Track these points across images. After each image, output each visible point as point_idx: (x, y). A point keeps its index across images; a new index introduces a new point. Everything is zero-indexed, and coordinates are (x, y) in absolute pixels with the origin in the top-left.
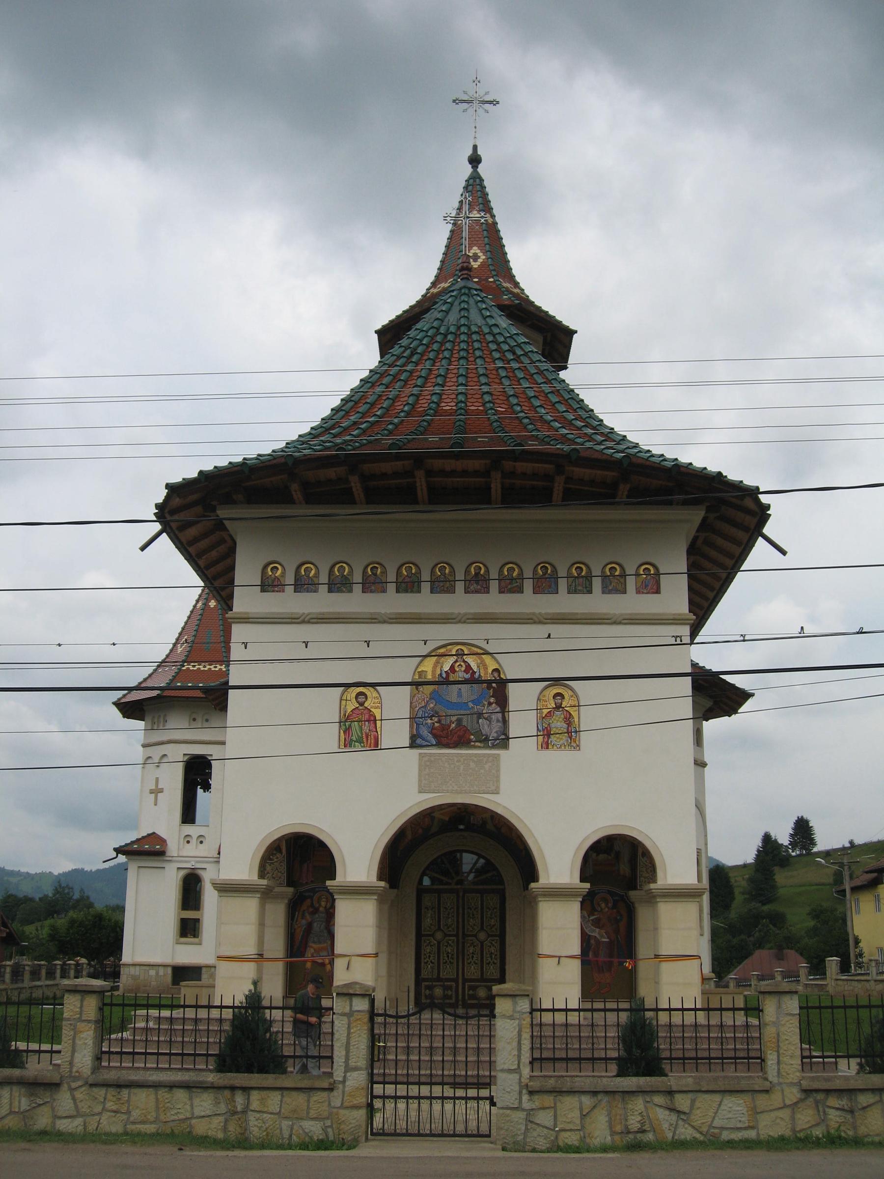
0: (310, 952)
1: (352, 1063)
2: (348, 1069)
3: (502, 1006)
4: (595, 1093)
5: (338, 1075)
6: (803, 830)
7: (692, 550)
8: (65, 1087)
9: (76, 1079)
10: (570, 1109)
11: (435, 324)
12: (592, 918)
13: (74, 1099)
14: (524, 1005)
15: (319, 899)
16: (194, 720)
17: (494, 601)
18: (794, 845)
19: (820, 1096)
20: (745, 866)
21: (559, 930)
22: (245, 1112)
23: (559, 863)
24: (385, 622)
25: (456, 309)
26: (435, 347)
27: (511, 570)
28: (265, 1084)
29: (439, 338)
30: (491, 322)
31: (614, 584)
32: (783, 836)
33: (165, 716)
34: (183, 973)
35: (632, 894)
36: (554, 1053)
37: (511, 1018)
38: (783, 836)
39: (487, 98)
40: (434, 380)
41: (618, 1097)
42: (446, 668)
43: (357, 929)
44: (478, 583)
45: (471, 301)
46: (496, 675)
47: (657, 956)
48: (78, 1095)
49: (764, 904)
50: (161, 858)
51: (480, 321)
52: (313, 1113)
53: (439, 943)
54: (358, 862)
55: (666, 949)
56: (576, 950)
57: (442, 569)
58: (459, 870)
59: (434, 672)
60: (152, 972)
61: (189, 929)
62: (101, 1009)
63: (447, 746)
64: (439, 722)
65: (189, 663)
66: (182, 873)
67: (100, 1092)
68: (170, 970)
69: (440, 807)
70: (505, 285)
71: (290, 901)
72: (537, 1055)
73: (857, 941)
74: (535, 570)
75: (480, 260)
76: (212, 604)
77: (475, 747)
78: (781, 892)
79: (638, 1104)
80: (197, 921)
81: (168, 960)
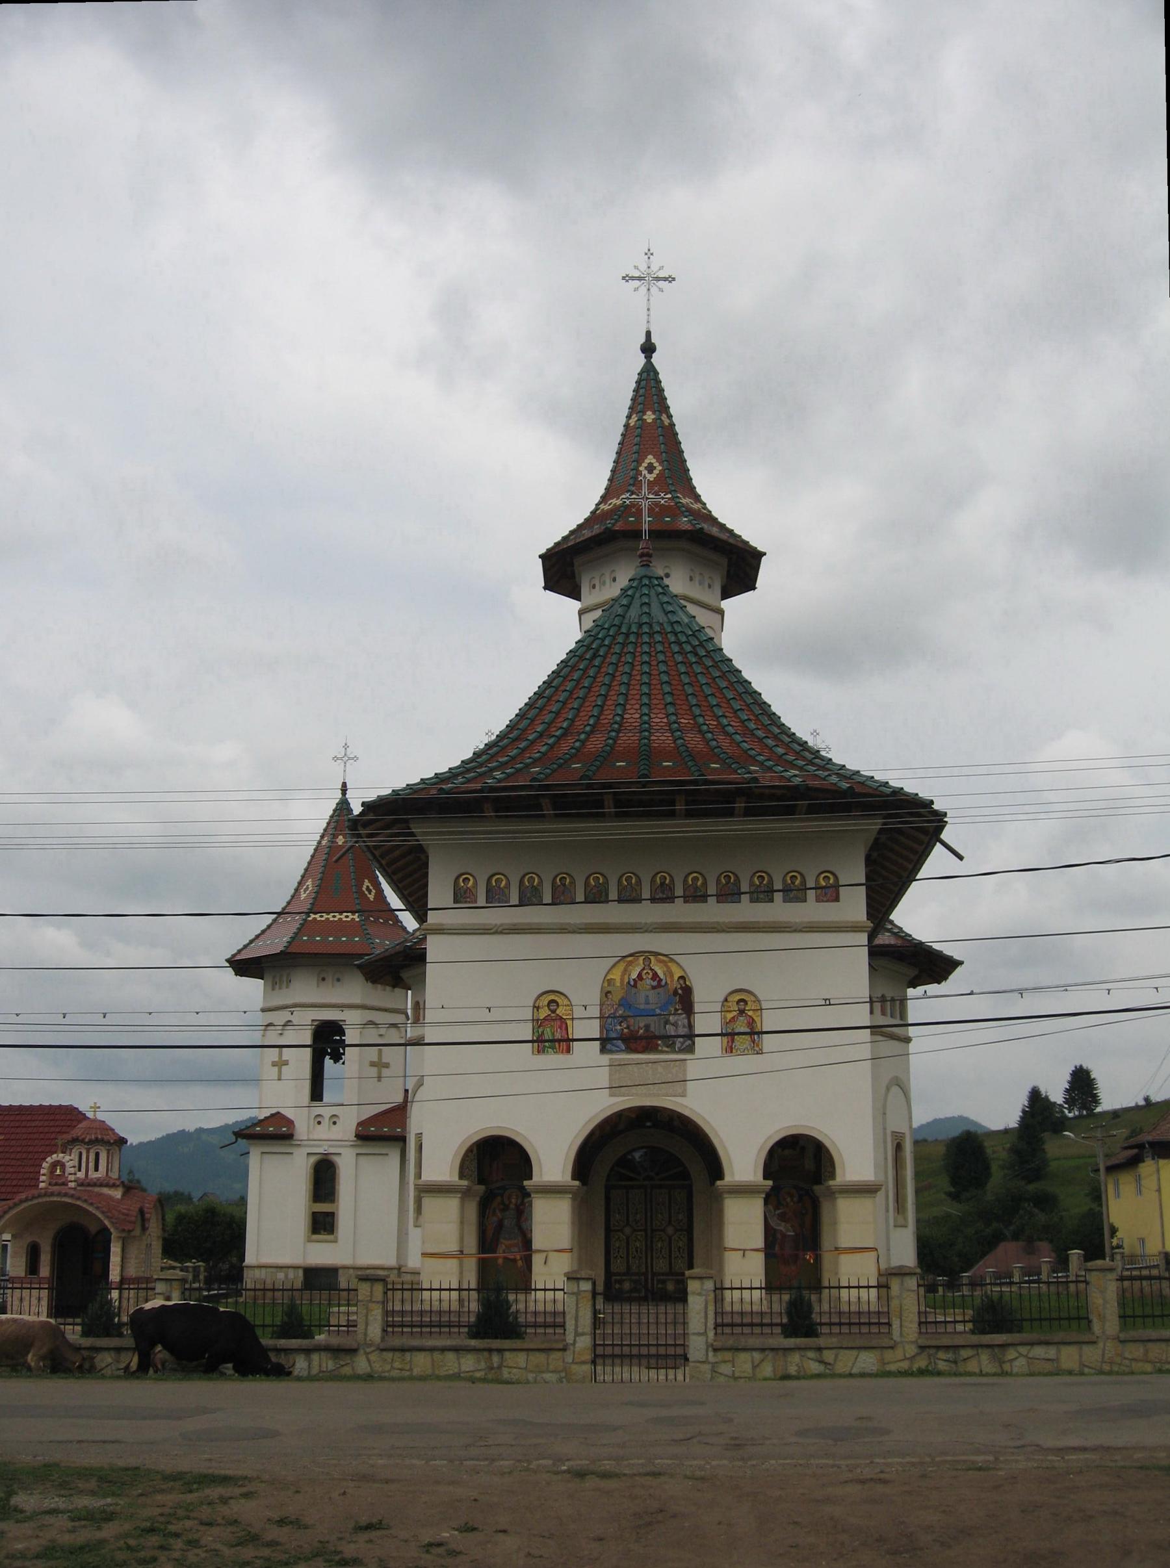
0: (501, 1248)
1: (580, 1330)
2: (577, 1334)
3: (693, 1286)
4: (763, 1350)
5: (570, 1338)
6: (1082, 1084)
7: (869, 861)
8: (362, 1351)
9: (370, 1345)
10: (744, 1362)
11: (617, 622)
12: (778, 1212)
13: (369, 1360)
14: (709, 1285)
15: (509, 1198)
16: (324, 979)
17: (678, 912)
18: (1070, 1101)
19: (932, 1351)
20: (1006, 1131)
21: (744, 1225)
22: (500, 1367)
23: (743, 1162)
24: (574, 932)
25: (637, 603)
26: (617, 649)
27: (695, 879)
28: (514, 1346)
29: (620, 639)
30: (674, 618)
31: (795, 893)
32: (1056, 1094)
33: (288, 975)
34: (319, 1279)
35: (816, 1188)
36: (731, 1327)
37: (699, 1294)
38: (1056, 1094)
39: (661, 274)
40: (617, 688)
41: (780, 1353)
42: (634, 975)
43: (553, 1225)
44: (663, 894)
45: (653, 593)
46: (682, 982)
47: (837, 1249)
48: (373, 1357)
49: (1030, 1182)
50: (287, 1142)
51: (662, 618)
52: (551, 1367)
53: (628, 1238)
54: (553, 1163)
55: (844, 1242)
56: (760, 1244)
57: (629, 879)
58: (648, 1170)
59: (622, 980)
60: (281, 1275)
61: (322, 1224)
62: (385, 1293)
63: (636, 1051)
64: (628, 1027)
65: (315, 913)
66: (313, 1159)
67: (389, 1355)
68: (301, 1273)
69: (630, 1109)
70: (684, 501)
71: (481, 1198)
72: (719, 1320)
73: (1114, 1231)
74: (718, 880)
75: (656, 472)
76: (340, 840)
77: (662, 1052)
78: (1053, 1165)
79: (796, 1358)
80: (331, 1215)
81: (298, 1260)
